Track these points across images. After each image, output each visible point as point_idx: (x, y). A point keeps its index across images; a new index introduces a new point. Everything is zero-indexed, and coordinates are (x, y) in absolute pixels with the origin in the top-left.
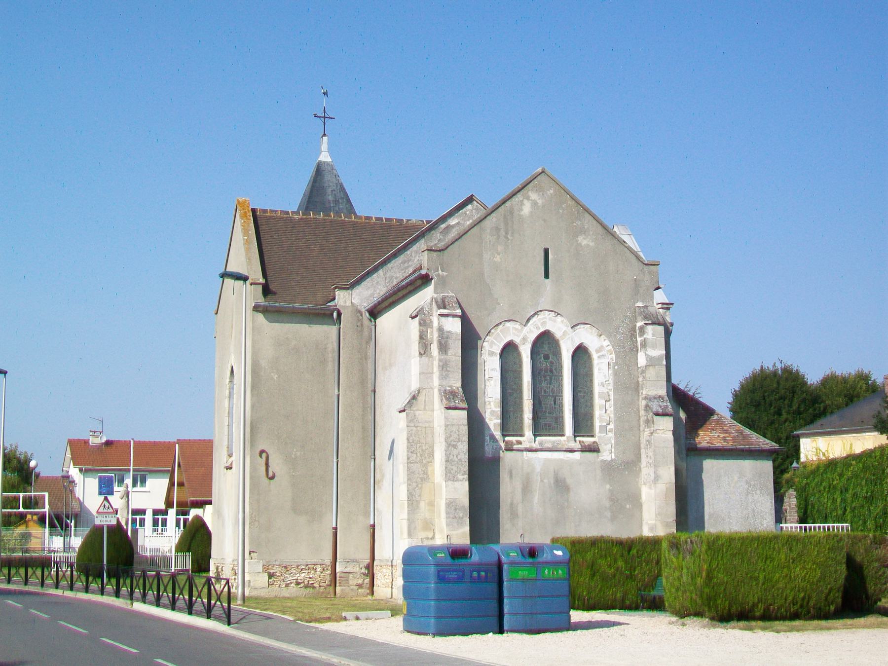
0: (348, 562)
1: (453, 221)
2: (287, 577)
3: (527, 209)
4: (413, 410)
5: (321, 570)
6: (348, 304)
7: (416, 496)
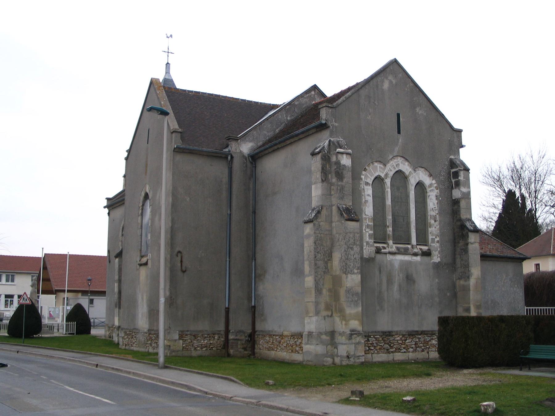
3: (386, 85)
4: (318, 222)
6: (238, 151)
7: (321, 285)
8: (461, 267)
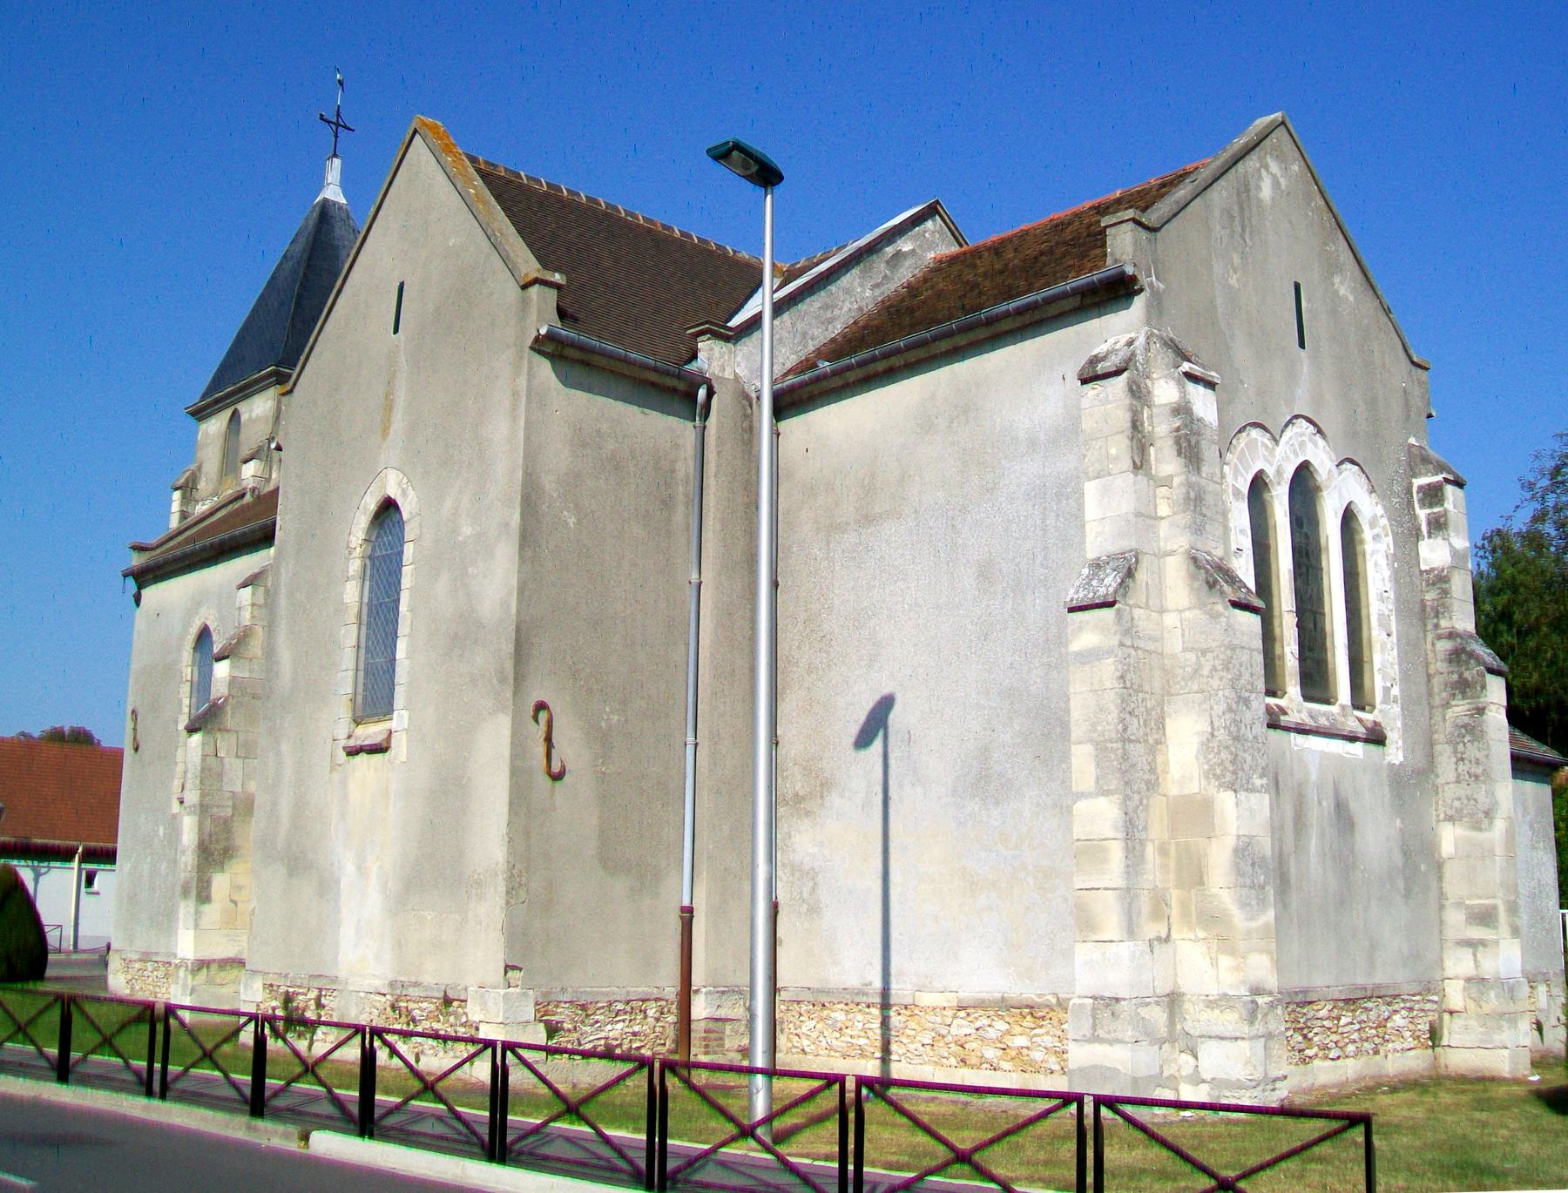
0: (723, 993)
1: (905, 245)
2: (586, 1032)
5: (658, 1015)
6: (728, 374)
8: (1458, 782)
